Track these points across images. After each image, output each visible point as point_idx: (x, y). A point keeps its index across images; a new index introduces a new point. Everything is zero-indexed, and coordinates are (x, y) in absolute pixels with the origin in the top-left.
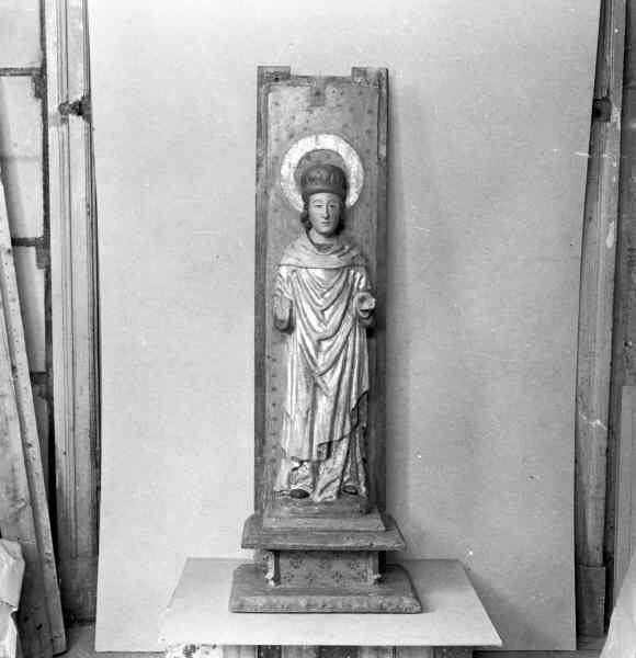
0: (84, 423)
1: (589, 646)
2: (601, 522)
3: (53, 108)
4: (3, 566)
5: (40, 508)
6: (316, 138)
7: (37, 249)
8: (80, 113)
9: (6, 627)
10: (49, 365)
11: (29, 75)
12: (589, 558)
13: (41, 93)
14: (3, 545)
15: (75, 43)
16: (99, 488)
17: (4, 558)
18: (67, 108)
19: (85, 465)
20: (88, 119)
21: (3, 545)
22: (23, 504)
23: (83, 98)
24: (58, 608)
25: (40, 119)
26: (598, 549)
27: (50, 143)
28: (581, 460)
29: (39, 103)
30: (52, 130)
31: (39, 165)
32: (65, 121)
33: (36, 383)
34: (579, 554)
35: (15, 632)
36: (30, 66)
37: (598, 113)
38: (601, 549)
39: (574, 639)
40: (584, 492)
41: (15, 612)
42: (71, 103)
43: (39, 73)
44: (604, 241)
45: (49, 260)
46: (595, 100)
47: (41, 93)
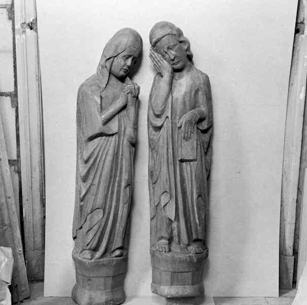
0: (36, 185)
1: (285, 295)
2: (293, 235)
3: (18, 26)
4: (2, 262)
5: (15, 228)
6: (190, 163)
7: (11, 98)
8: (31, 29)
9: (5, 294)
10: (19, 156)
11: (6, 8)
12: (286, 251)
13: (11, 17)
14: (2, 251)
15: (103, 158)
16: (45, 217)
17: (3, 259)
18: (25, 25)
19: (38, 207)
20: (36, 31)
21: (2, 251)
22: (6, 227)
23: (33, 20)
24: (28, 278)
25: (12, 31)
26: (290, 248)
27: (16, 44)
28: (285, 204)
29: (10, 23)
30: (17, 37)
31: (11, 55)
32: (24, 32)
33: (13, 165)
34: (282, 250)
35: (10, 295)
36: (5, 3)
37: (297, 31)
38: (292, 248)
39: (278, 293)
40: (285, 220)
41: (10, 285)
42: (27, 22)
43: (10, 7)
44: (299, 96)
45: (18, 104)
46: (297, 23)
47: (11, 17)
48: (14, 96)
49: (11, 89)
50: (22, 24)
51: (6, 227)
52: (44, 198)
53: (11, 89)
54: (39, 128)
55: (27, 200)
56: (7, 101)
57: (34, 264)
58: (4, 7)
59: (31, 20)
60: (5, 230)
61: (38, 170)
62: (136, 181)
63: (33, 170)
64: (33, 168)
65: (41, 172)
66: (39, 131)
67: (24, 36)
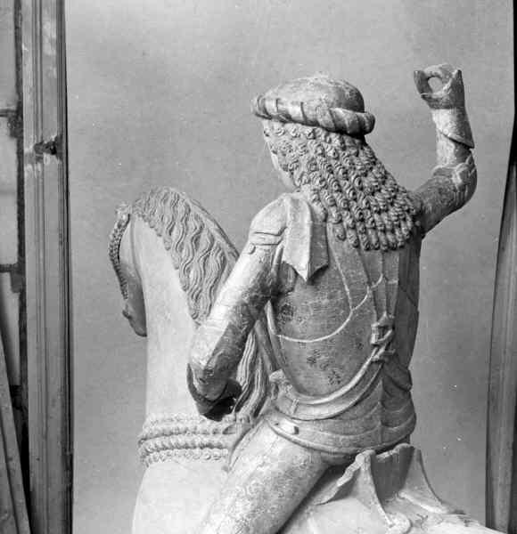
0: (56, 431)
3: (28, 149)
11: (6, 116)
13: (16, 131)
22: (7, 515)
23: (56, 138)
30: (28, 168)
32: (39, 159)
42: (46, 142)
45: (24, 285)
48: (18, 270)
49: (11, 258)
50: (37, 145)
51: (7, 515)
52: (68, 453)
53: (11, 258)
54: (63, 350)
55: (38, 459)
56: (7, 277)
57: (446, 87)
58: (4, 114)
59: (53, 138)
60: (4, 521)
61: (58, 405)
62: (454, 124)
63: (50, 403)
64: (50, 399)
65: (64, 420)
66: (61, 228)
67: (39, 166)
